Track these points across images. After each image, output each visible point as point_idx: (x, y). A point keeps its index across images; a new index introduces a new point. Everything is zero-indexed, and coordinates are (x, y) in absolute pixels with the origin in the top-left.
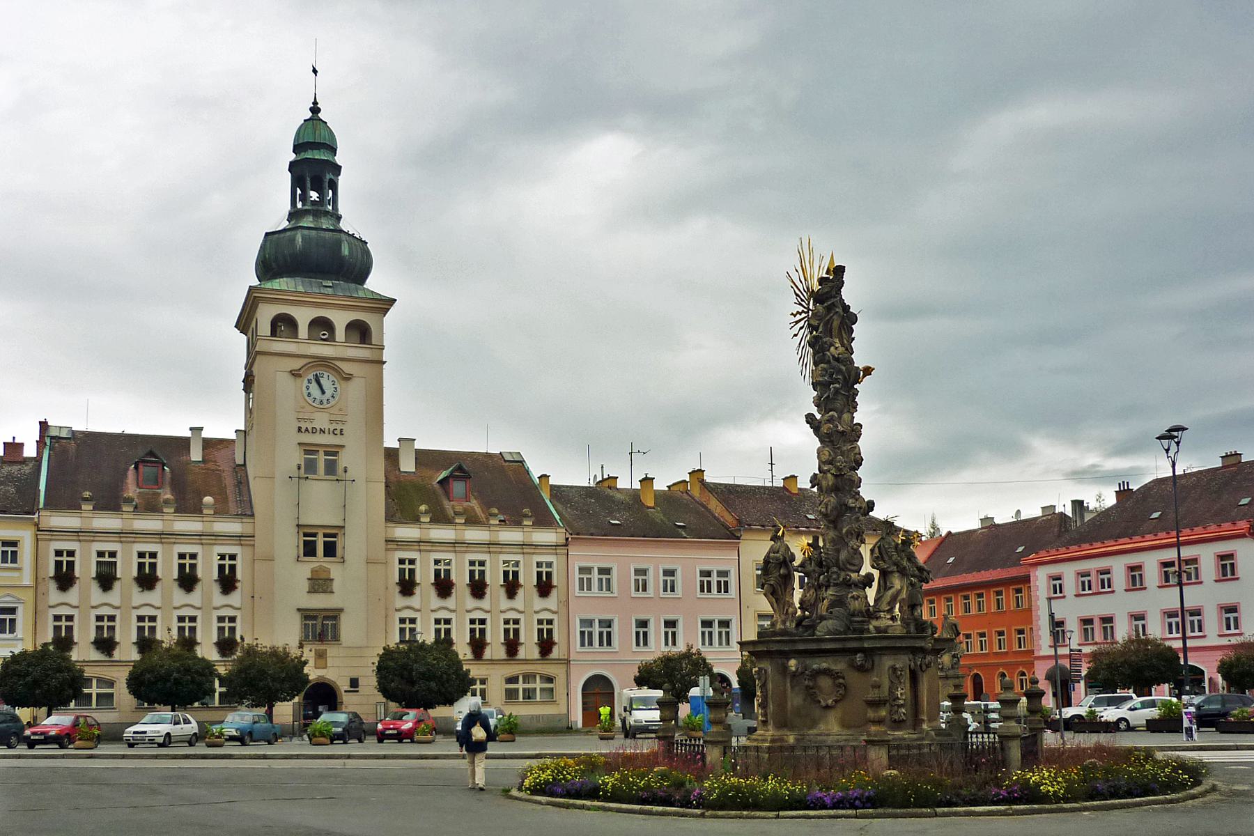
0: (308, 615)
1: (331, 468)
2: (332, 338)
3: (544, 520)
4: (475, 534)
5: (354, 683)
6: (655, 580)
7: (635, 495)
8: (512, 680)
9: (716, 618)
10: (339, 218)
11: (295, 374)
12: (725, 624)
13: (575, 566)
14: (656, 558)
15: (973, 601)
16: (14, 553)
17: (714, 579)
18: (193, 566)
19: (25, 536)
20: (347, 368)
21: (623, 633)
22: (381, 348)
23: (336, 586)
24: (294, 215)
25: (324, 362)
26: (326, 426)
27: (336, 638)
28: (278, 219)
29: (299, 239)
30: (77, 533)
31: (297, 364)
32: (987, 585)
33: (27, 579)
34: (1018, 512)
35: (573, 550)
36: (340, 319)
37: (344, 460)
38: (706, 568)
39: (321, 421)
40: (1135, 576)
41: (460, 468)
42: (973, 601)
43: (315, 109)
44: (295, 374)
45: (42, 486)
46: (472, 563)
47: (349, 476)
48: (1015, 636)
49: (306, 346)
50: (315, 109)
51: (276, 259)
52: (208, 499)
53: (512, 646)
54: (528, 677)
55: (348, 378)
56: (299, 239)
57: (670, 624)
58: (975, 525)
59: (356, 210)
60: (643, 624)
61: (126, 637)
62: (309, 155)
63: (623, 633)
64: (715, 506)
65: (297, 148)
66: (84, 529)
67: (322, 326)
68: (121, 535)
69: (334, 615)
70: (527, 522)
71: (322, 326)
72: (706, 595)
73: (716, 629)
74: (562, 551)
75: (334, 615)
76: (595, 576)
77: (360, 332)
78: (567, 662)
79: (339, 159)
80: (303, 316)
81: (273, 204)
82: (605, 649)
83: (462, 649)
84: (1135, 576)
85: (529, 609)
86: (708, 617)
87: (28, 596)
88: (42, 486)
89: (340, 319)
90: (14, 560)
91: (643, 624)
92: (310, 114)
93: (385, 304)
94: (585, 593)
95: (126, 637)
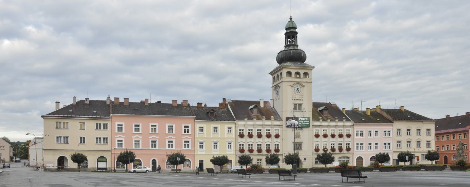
0: (295, 144)
1: (300, 109)
2: (300, 77)
3: (348, 120)
4: (333, 123)
5: (305, 159)
6: (373, 133)
7: (364, 112)
8: (340, 158)
9: (387, 142)
10: (297, 46)
11: (292, 86)
12: (389, 144)
13: (355, 130)
14: (373, 128)
15: (445, 137)
16: (202, 130)
17: (359, 133)
18: (243, 132)
19: (233, 126)
20: (303, 84)
21: (366, 146)
22: (311, 79)
23: (301, 136)
24: (285, 47)
25: (299, 83)
26: (299, 98)
27: (301, 149)
28: (282, 47)
29: (292, 52)
30: (262, 125)
31: (292, 84)
32: (456, 132)
33: (234, 137)
34: (458, 114)
35: (355, 127)
36: (302, 72)
37: (303, 107)
38: (385, 130)
39: (298, 97)
40: (399, 132)
41: (326, 107)
42: (445, 137)
43: (291, 19)
44: (292, 86)
45: (233, 114)
46: (258, 130)
47: (305, 110)
48: (442, 147)
49: (294, 79)
50: (291, 19)
51: (283, 58)
52: (272, 117)
53: (341, 150)
54: (344, 157)
55: (304, 86)
56: (292, 52)
57: (376, 144)
58: (445, 117)
59: (302, 44)
60: (370, 144)
61: (264, 149)
62: (288, 31)
63: (366, 146)
64: (385, 115)
65: (287, 29)
66: (246, 125)
67: (298, 73)
68: (253, 125)
69: (300, 144)
70: (337, 120)
71: (298, 73)
72: (385, 137)
73: (387, 145)
74: (352, 127)
75: (300, 144)
76: (387, 133)
77: (306, 74)
78: (353, 153)
79: (297, 30)
80: (293, 72)
81: (279, 43)
82: (361, 150)
83: (329, 151)
84: (399, 132)
85: (345, 140)
86: (385, 142)
87: (234, 140)
88: (233, 114)
89: (302, 72)
90: (216, 132)
91: (370, 144)
92: (289, 20)
93: (312, 68)
94: (357, 137)
95: (264, 149)
